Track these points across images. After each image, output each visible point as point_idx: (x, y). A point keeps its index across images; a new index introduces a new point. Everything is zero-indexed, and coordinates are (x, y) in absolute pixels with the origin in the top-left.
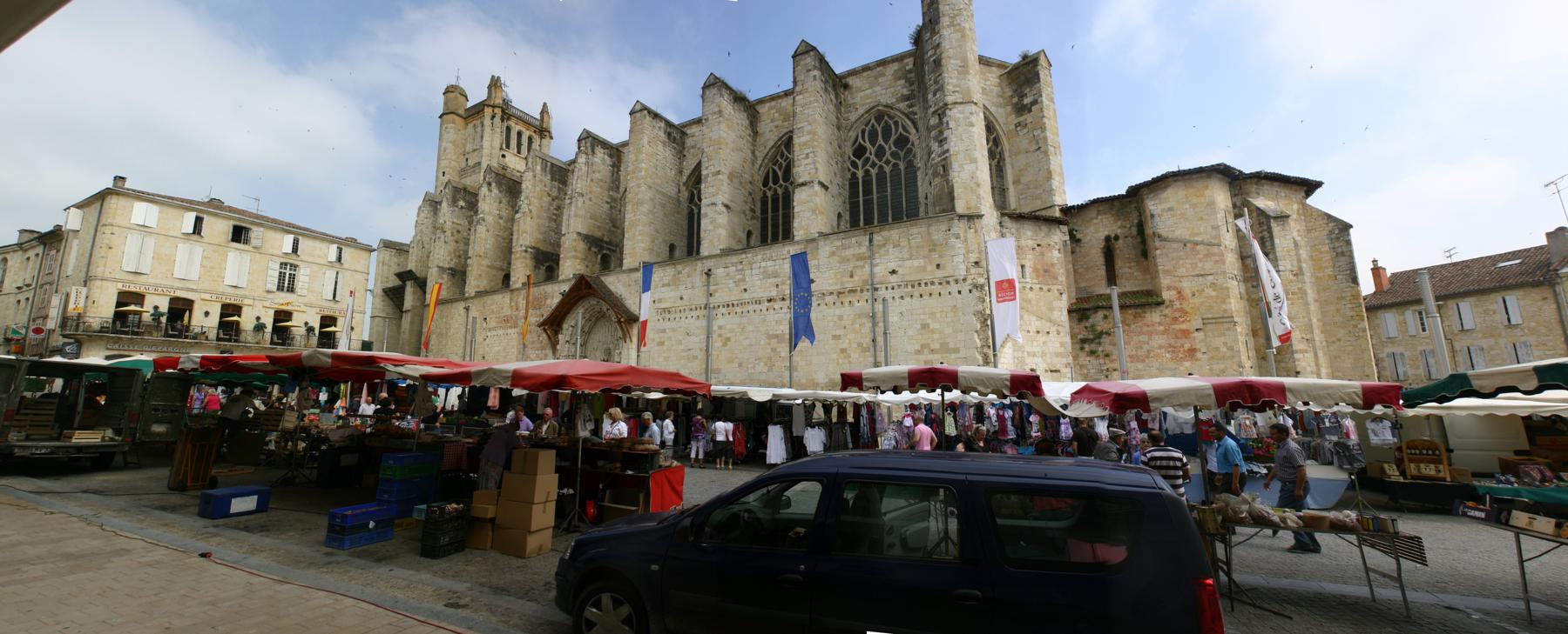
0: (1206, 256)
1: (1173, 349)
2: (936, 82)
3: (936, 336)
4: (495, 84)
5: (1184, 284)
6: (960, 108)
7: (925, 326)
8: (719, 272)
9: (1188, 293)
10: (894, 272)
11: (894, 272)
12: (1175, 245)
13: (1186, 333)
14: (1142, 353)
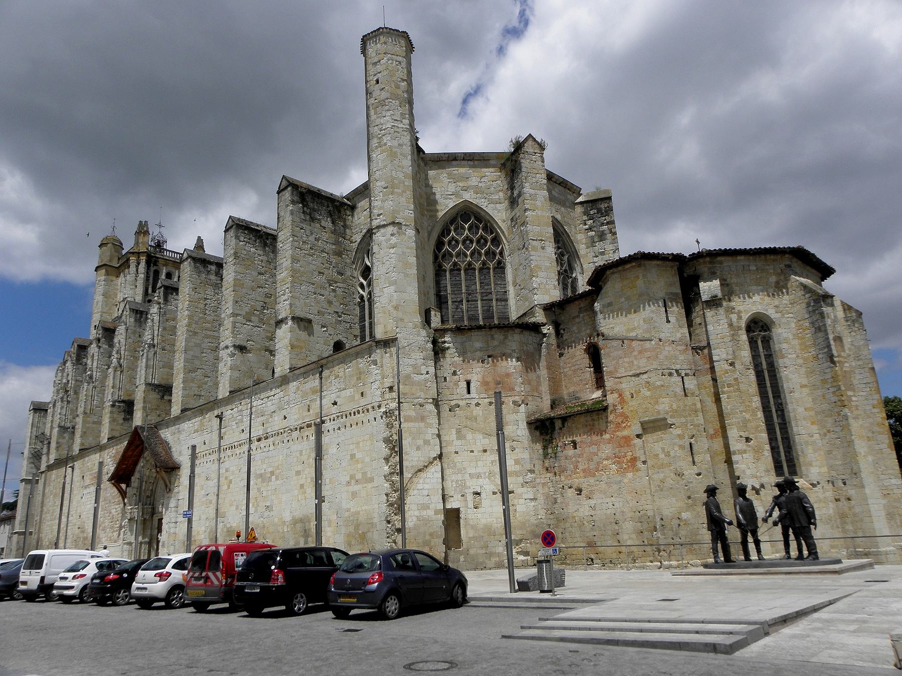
0: (640, 352)
1: (617, 458)
2: (169, 276)
3: (359, 466)
4: (142, 230)
5: (624, 386)
6: (382, 230)
7: (353, 456)
8: (228, 413)
9: (627, 395)
10: (335, 403)
11: (335, 403)
12: (615, 343)
13: (627, 439)
14: (592, 466)
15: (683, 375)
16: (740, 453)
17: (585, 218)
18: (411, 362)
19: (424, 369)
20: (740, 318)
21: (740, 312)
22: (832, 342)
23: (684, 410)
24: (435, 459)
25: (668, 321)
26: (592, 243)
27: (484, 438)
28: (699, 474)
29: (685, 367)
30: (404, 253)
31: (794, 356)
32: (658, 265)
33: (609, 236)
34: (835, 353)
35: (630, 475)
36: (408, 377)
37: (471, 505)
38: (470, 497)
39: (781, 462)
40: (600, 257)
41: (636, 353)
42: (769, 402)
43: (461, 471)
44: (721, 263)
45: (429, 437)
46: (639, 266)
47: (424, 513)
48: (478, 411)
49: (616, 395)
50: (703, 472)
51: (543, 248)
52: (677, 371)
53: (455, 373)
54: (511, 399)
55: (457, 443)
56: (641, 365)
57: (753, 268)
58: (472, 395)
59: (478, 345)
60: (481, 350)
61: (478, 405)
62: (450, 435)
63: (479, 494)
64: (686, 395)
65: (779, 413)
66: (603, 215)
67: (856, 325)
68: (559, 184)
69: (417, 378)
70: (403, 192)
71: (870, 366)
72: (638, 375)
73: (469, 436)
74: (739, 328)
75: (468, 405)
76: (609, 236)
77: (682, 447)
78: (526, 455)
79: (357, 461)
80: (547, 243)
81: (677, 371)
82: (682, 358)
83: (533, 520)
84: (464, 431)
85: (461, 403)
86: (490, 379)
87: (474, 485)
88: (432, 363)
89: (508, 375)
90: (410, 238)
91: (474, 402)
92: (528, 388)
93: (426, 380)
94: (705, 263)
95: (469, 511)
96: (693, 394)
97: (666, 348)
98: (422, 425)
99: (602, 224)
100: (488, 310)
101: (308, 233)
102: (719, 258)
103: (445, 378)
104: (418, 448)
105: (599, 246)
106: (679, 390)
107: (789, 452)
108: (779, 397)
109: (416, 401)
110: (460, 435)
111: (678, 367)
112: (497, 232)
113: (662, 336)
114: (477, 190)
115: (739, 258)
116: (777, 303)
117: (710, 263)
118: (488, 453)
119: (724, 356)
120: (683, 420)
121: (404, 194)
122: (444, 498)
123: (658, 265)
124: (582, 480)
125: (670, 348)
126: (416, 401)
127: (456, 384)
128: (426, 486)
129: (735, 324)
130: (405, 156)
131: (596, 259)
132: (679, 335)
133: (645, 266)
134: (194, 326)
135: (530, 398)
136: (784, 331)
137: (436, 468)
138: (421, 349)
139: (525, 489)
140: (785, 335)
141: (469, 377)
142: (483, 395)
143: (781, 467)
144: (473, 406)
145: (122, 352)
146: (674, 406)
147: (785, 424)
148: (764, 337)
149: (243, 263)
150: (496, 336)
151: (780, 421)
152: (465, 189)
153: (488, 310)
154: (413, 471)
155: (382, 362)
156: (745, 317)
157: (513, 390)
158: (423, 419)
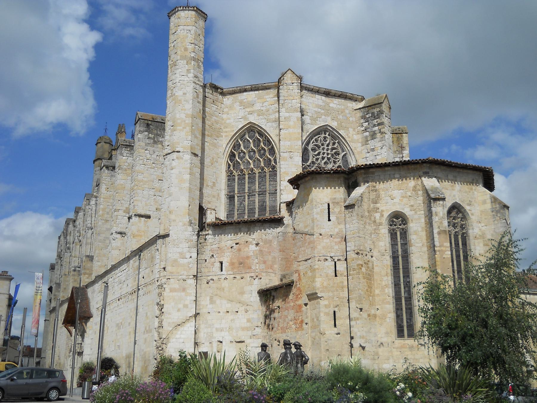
5: (301, 268)
15: (336, 260)
16: (355, 320)
17: (362, 121)
18: (179, 250)
19: (188, 256)
20: (382, 216)
21: (382, 211)
22: (436, 235)
25: (329, 220)
26: (366, 142)
27: (228, 303)
28: (339, 334)
29: (338, 254)
30: (180, 172)
31: (421, 245)
32: (309, 180)
33: (378, 135)
34: (437, 243)
35: (300, 332)
36: (175, 261)
38: (215, 344)
39: (403, 327)
40: (371, 153)
41: (307, 244)
42: (400, 281)
45: (187, 302)
46: (312, 179)
48: (225, 284)
49: (297, 275)
50: (342, 333)
51: (291, 158)
54: (249, 275)
55: (210, 306)
56: (309, 253)
58: (223, 272)
62: (204, 301)
63: (221, 342)
64: (336, 276)
65: (407, 289)
66: (375, 118)
67: (499, 215)
72: (306, 260)
73: (218, 302)
74: (381, 224)
76: (378, 135)
77: (327, 314)
79: (500, 279)
80: (296, 154)
81: (331, 257)
82: (336, 247)
84: (215, 298)
85: (214, 278)
86: (235, 261)
87: (218, 336)
89: (248, 257)
90: (186, 161)
91: (224, 277)
93: (189, 263)
96: (341, 275)
97: (325, 241)
98: (183, 294)
99: (375, 126)
100: (263, 205)
101: (151, 152)
102: (371, 170)
103: (206, 260)
104: (179, 310)
105: (372, 144)
106: (331, 272)
107: (410, 320)
108: (408, 276)
109: (180, 277)
110: (212, 301)
111: (332, 255)
112: (272, 145)
113: (322, 232)
114: (260, 113)
115: (386, 169)
116: (412, 203)
118: (230, 313)
119: (353, 248)
120: (331, 294)
121: (185, 130)
122: (196, 344)
124: (280, 335)
125: (328, 241)
126: (180, 277)
127: (213, 264)
129: (378, 221)
130: (187, 101)
131: (368, 155)
132: (337, 230)
134: (106, 216)
135: (264, 274)
136: (414, 225)
137: (192, 323)
138: (188, 240)
139: (252, 340)
140: (415, 228)
143: (403, 330)
144: (222, 280)
145: (81, 232)
146: (325, 284)
147: (410, 298)
148: (403, 229)
149: (125, 172)
151: (406, 295)
152: (251, 113)
153: (263, 205)
154: (173, 326)
155: (161, 250)
156: (386, 215)
157: (250, 268)
158: (184, 290)
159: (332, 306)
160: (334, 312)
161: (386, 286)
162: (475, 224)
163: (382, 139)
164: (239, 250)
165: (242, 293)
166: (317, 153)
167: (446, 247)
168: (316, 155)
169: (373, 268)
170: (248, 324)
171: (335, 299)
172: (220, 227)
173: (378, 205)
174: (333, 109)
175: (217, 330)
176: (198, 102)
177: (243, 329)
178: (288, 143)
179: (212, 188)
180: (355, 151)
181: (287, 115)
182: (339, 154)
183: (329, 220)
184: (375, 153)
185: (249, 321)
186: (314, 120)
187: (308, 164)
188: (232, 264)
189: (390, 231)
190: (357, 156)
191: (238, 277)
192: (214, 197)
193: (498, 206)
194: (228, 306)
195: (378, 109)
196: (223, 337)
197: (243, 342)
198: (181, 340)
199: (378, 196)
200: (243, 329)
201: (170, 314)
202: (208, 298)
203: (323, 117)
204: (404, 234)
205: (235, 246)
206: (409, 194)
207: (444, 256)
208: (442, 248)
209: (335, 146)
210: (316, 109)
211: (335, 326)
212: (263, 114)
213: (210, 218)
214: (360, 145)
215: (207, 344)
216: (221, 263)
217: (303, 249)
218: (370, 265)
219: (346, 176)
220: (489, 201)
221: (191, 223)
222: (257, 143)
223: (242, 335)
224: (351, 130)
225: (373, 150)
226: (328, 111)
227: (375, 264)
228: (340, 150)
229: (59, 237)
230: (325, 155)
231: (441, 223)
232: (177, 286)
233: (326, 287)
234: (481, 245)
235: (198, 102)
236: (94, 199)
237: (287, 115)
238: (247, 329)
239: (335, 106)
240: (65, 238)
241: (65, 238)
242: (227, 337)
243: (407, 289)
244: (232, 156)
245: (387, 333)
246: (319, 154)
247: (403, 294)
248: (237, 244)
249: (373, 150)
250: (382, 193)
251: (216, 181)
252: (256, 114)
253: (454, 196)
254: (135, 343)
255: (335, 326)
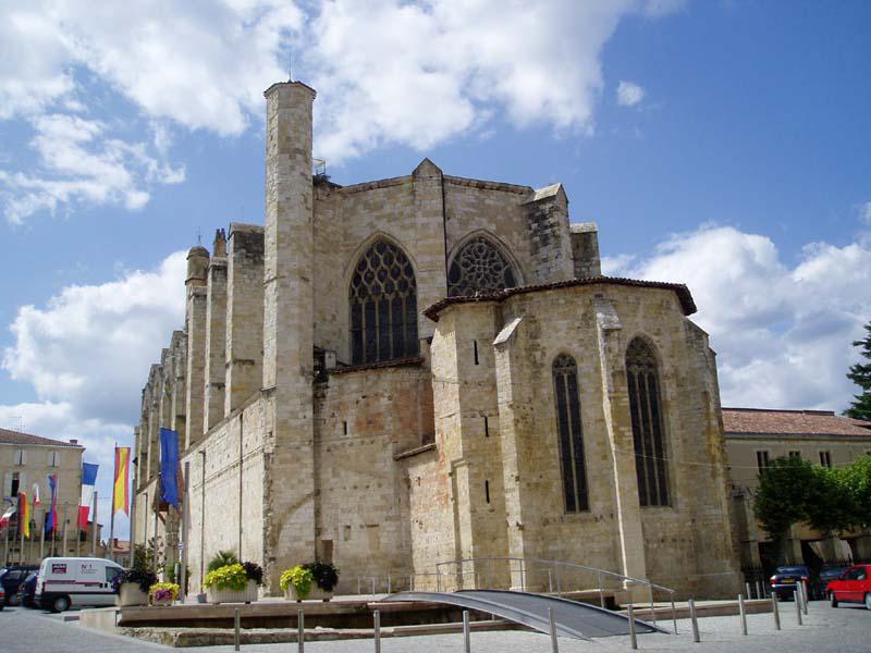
17: (530, 221)
18: (289, 408)
19: (301, 415)
20: (544, 354)
23: (484, 450)
24: (309, 496)
25: (477, 363)
26: (535, 250)
28: (492, 511)
37: (342, 538)
38: (341, 530)
43: (335, 506)
44: (531, 298)
45: (303, 476)
47: (295, 544)
48: (351, 451)
52: (481, 412)
53: (333, 415)
55: (333, 480)
57: (562, 301)
58: (348, 435)
59: (354, 387)
60: (357, 391)
61: (351, 445)
62: (327, 475)
63: (349, 527)
64: (487, 435)
68: (497, 189)
69: (293, 422)
70: (289, 245)
71: (703, 390)
73: (343, 474)
75: (343, 445)
76: (552, 240)
78: (391, 491)
81: (481, 412)
83: (395, 551)
87: (345, 519)
88: (310, 407)
89: (379, 414)
91: (348, 442)
92: (399, 425)
93: (303, 425)
94: (516, 300)
95: (340, 543)
98: (296, 465)
102: (529, 295)
104: (292, 487)
110: (335, 474)
111: (482, 407)
114: (391, 218)
116: (581, 336)
117: (520, 300)
119: (505, 398)
123: (473, 307)
128: (299, 521)
129: (538, 362)
131: (539, 268)
133: (458, 310)
140: (586, 370)
141: (345, 419)
142: (356, 435)
146: (474, 447)
150: (370, 377)
158: (298, 460)
159: (483, 475)
160: (487, 483)
161: (552, 446)
162: (665, 359)
163: (558, 246)
164: (368, 405)
165: (373, 462)
166: (469, 269)
167: (623, 392)
168: (494, 261)
169: (534, 423)
170: (383, 503)
171: (488, 465)
172: (343, 369)
173: (539, 341)
174: (489, 206)
175: (343, 511)
176: (307, 208)
177: (377, 508)
178: (428, 258)
179: (331, 322)
180: (522, 264)
181: (425, 220)
182: (500, 269)
183: (477, 363)
184: (548, 264)
185: (383, 497)
186: (464, 224)
187: (458, 284)
188: (359, 424)
189: (554, 373)
190: (524, 269)
191: (367, 440)
192: (334, 334)
193: (693, 334)
194: (355, 479)
195: (551, 205)
196: (351, 520)
197: (377, 526)
198: (298, 526)
199: (538, 329)
200: (377, 508)
201: (281, 492)
202: (330, 470)
203: (477, 218)
204: (573, 378)
205: (362, 401)
206: (577, 324)
207: (622, 404)
208: (619, 394)
209: (495, 258)
210: (467, 209)
211: (488, 500)
212: (396, 219)
213: (330, 362)
214: (528, 254)
215: (331, 530)
216: (345, 424)
217: (445, 401)
218: (530, 420)
219: (497, 304)
220: (682, 328)
221: (303, 372)
222: (389, 261)
223: (376, 517)
224: (515, 234)
225: (545, 260)
226: (483, 211)
227: (537, 417)
228: (502, 264)
229: (144, 391)
230: (482, 271)
231: (616, 361)
232: (289, 456)
233: (474, 451)
234: (674, 386)
235: (307, 208)
236: (184, 339)
237: (425, 220)
238: (381, 508)
239: (492, 202)
240: (151, 391)
241: (151, 391)
242: (356, 520)
243: (578, 448)
244: (356, 279)
245: (553, 506)
246: (473, 270)
247: (572, 455)
248: (364, 397)
249: (545, 260)
250: (543, 324)
251: (337, 311)
252: (385, 220)
253: (637, 324)
254: (241, 532)
255: (488, 500)
